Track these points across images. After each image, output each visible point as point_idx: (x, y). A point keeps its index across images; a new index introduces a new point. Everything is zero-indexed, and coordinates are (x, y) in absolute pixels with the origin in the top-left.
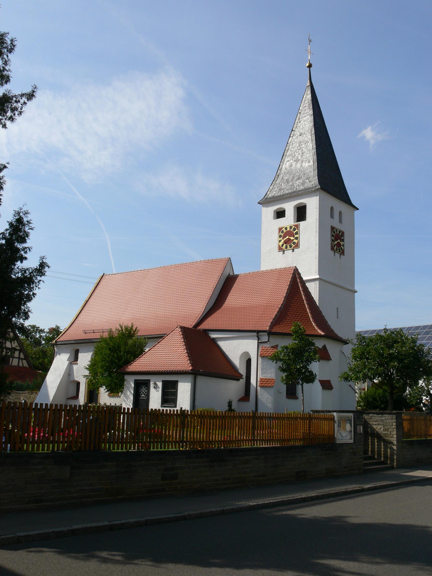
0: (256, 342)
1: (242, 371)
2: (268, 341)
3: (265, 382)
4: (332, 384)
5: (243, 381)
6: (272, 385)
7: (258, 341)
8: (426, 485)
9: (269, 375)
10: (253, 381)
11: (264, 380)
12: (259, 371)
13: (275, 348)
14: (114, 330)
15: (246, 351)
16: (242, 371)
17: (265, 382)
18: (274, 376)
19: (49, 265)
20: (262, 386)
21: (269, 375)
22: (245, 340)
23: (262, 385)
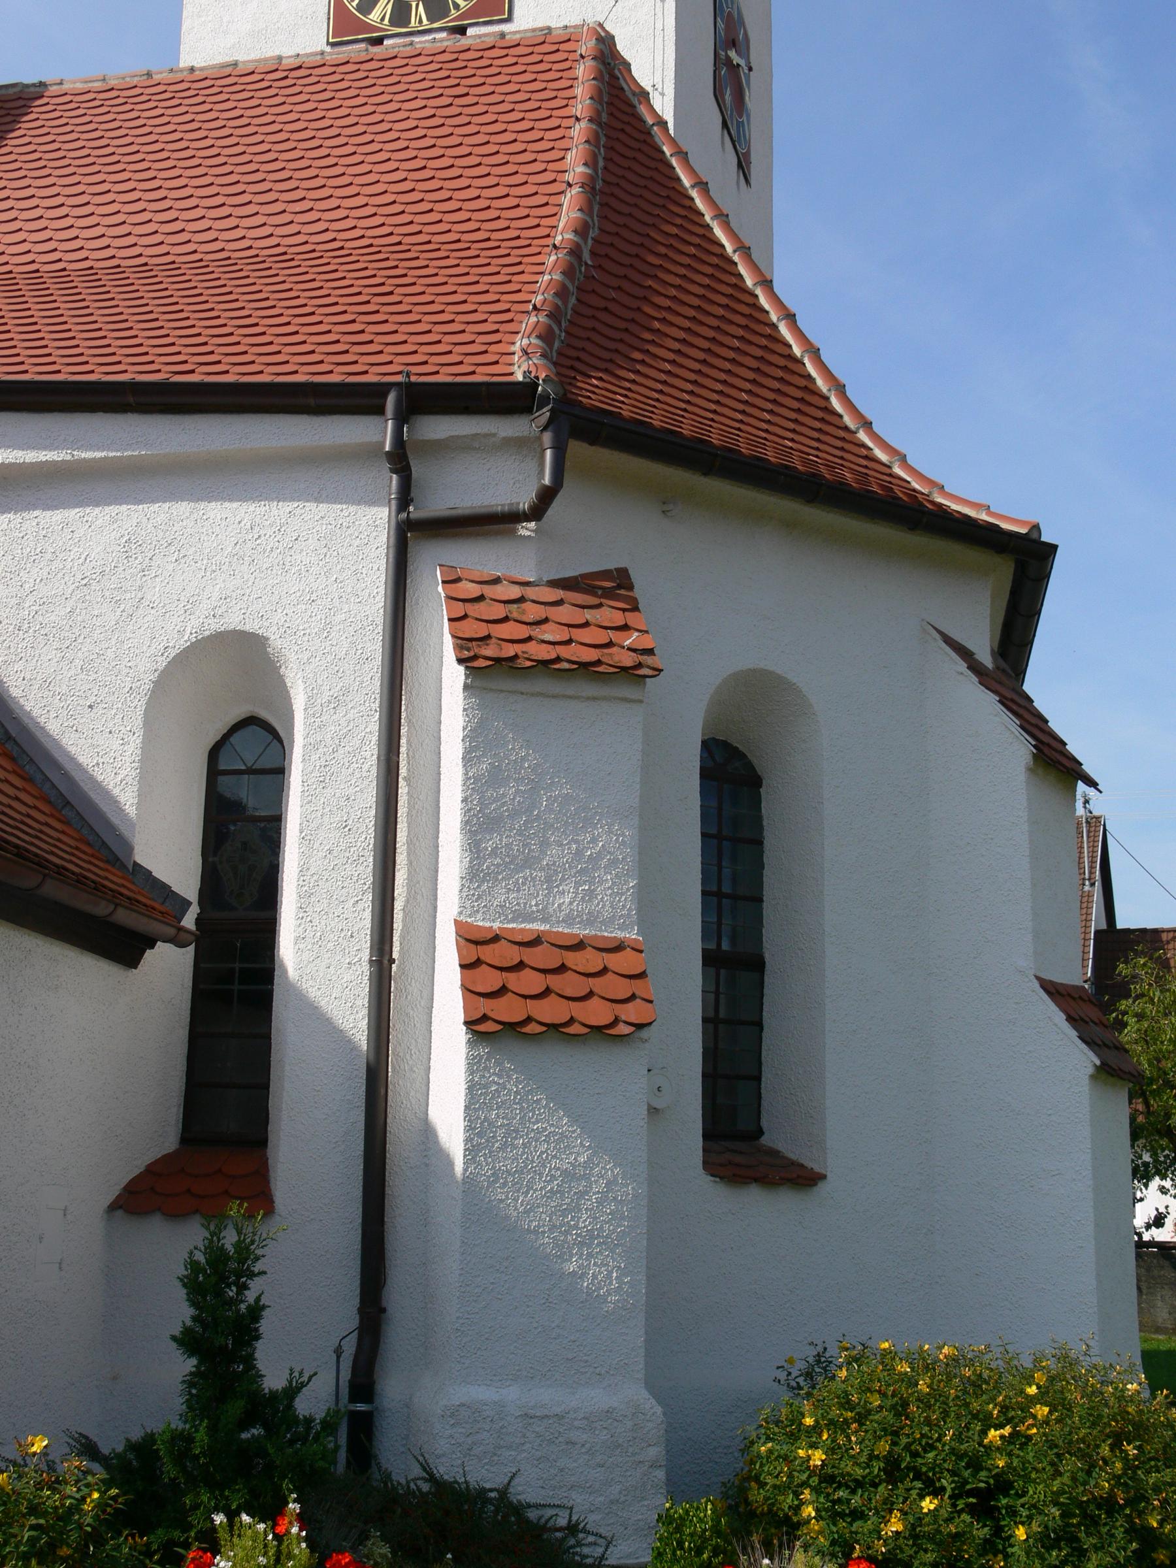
0: (370, 526)
1: (169, 850)
2: (537, 512)
3: (530, 982)
4: (1149, 927)
5: (169, 967)
6: (631, 1012)
7: (404, 499)
8: (270, 1061)
9: (566, 899)
10: (317, 948)
11: (509, 954)
12: (401, 858)
13: (609, 594)
14: (189, 1323)
15: (233, 621)
16: (169, 850)
17: (530, 982)
18: (627, 904)
19: (752, 182)
20: (512, 1028)
21: (566, 899)
22: (216, 510)
23: (507, 1010)
